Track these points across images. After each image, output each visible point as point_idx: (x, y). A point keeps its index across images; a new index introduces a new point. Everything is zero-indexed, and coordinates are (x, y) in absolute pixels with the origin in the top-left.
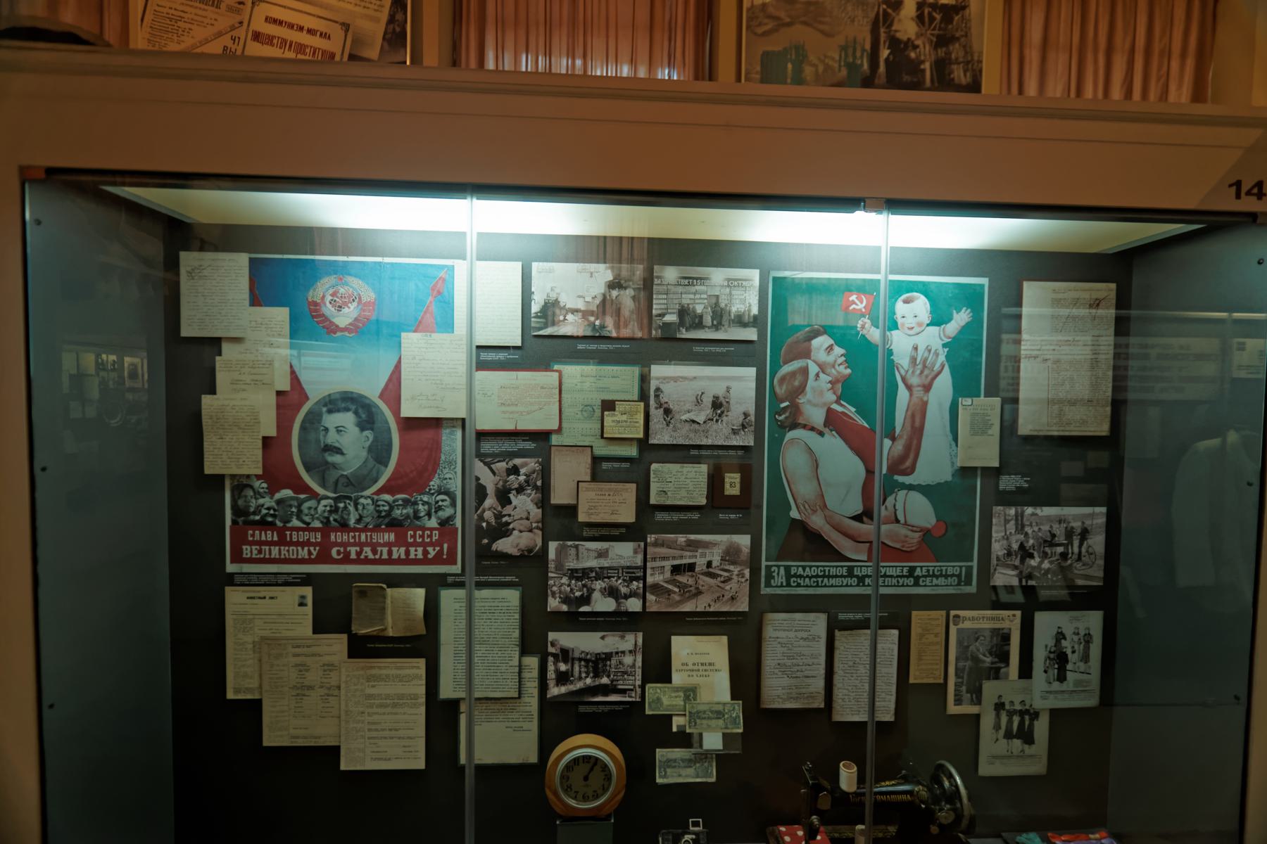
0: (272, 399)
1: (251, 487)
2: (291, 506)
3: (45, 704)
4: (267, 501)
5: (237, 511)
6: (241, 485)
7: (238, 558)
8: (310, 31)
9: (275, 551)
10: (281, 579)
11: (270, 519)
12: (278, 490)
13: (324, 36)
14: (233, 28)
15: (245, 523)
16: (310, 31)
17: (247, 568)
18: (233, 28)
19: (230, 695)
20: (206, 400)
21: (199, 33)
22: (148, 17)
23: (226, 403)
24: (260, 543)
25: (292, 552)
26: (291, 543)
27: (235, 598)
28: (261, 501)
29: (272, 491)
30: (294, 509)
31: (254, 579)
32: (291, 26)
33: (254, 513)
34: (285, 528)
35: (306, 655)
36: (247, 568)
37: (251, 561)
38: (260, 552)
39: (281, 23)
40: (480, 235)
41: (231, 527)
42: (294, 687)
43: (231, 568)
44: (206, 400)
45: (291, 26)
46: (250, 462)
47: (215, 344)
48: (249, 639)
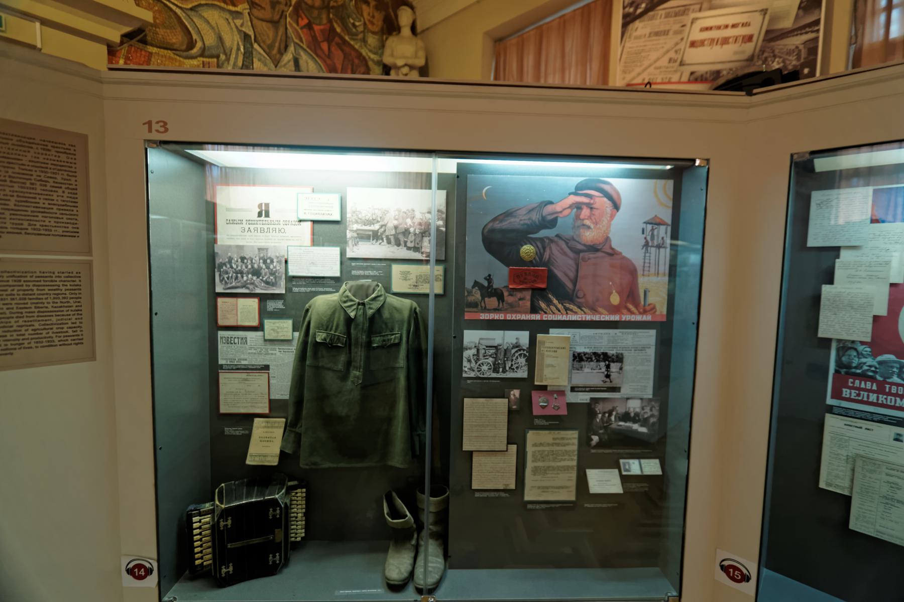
0: (886, 289)
1: (856, 349)
2: (893, 367)
3: (158, 447)
4: (869, 361)
5: (840, 365)
6: (845, 347)
7: (837, 395)
8: (734, 26)
9: (873, 397)
10: (876, 418)
11: (871, 374)
12: (880, 354)
13: (745, 25)
14: (677, 44)
15: (847, 373)
16: (734, 26)
17: (845, 404)
18: (677, 44)
19: (822, 485)
20: (826, 289)
21: (654, 55)
22: (624, 56)
23: (843, 290)
24: (859, 389)
25: (891, 400)
26: (890, 394)
27: (832, 423)
28: (864, 360)
29: (874, 355)
30: (895, 370)
31: (852, 413)
32: (719, 28)
33: (856, 368)
34: (885, 382)
35: (899, 478)
36: (845, 404)
37: (849, 400)
38: (859, 395)
39: (711, 28)
40: (439, 175)
41: (834, 375)
42: (884, 497)
43: (830, 401)
44: (826, 289)
45: (719, 28)
46: (862, 331)
47: (835, 251)
48: (844, 452)
